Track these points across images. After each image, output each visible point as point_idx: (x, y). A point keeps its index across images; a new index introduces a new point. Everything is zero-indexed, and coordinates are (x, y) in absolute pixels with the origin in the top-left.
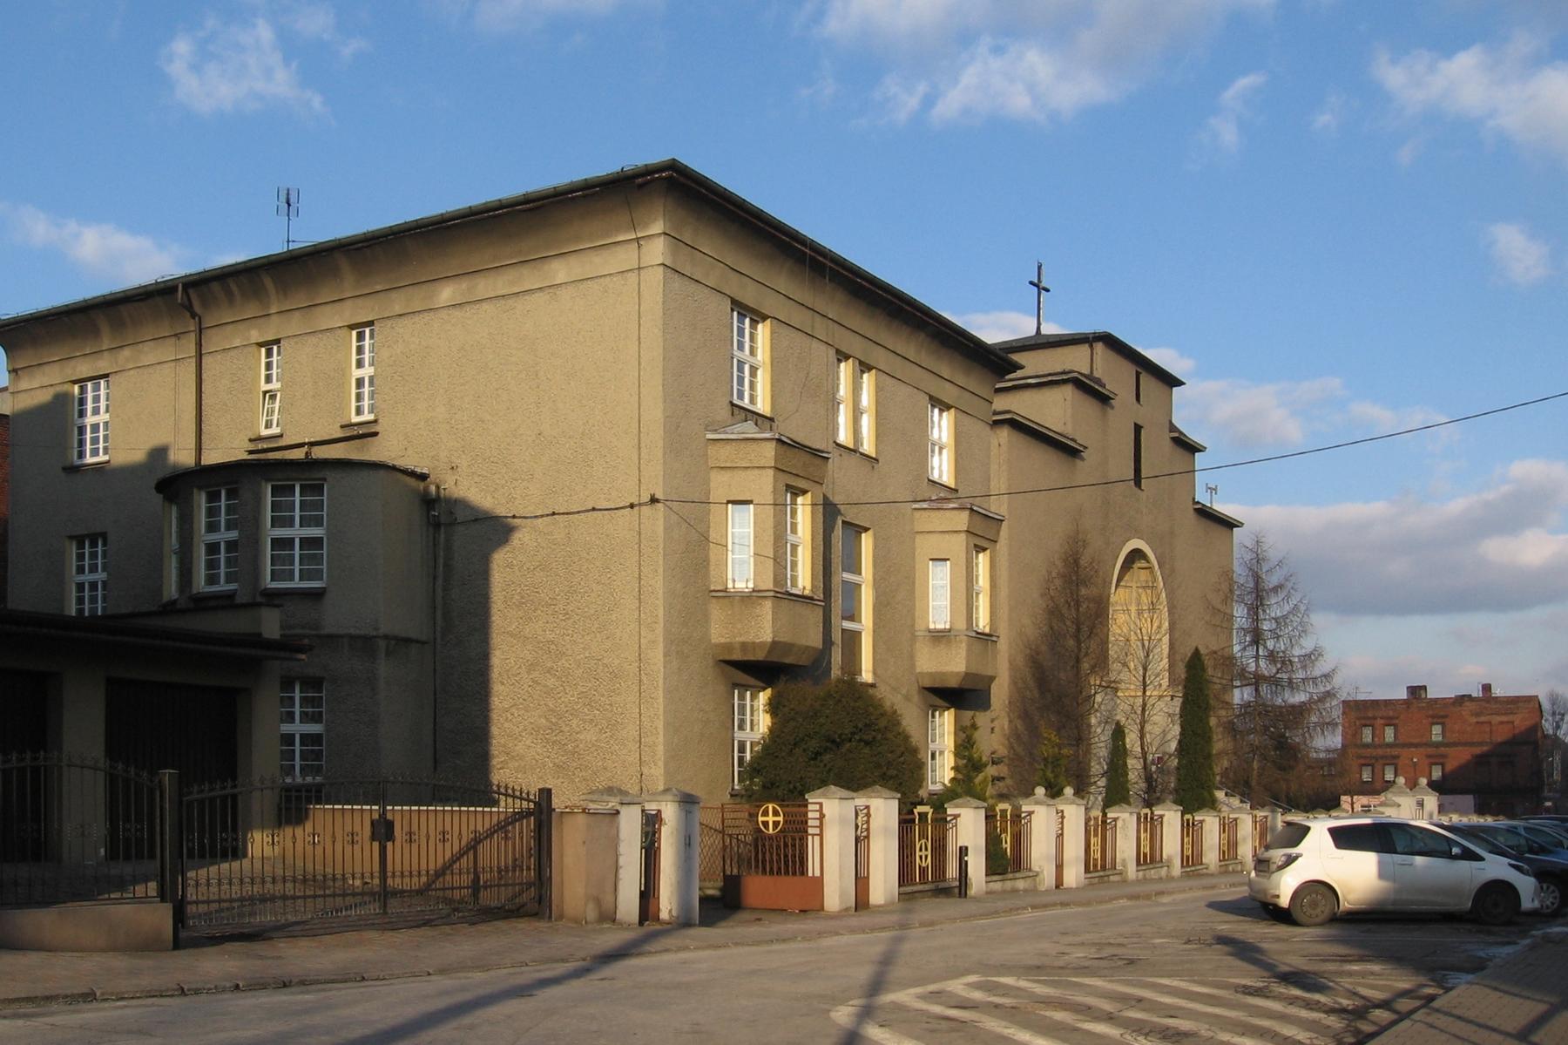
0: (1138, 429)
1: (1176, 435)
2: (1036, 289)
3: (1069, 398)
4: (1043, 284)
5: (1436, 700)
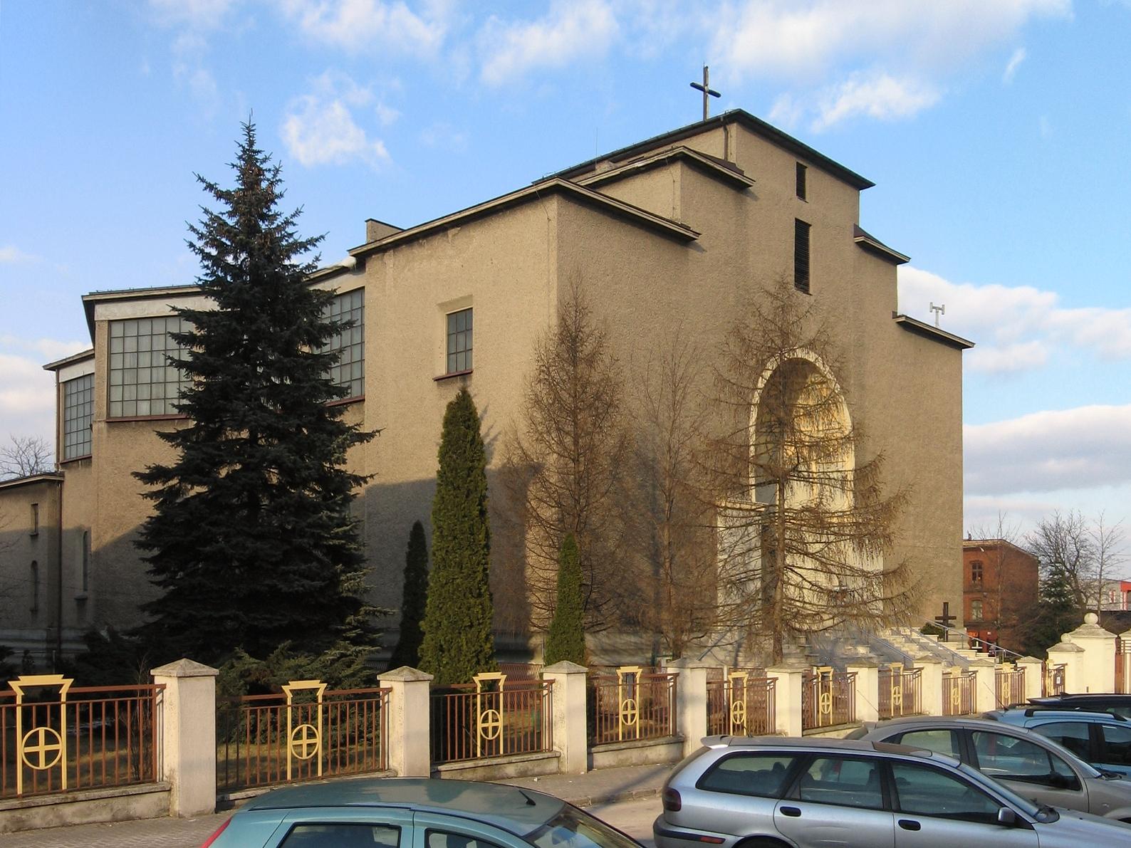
0: (802, 229)
1: (861, 239)
2: (702, 92)
3: (678, 179)
4: (710, 87)
5: (94, 307)
